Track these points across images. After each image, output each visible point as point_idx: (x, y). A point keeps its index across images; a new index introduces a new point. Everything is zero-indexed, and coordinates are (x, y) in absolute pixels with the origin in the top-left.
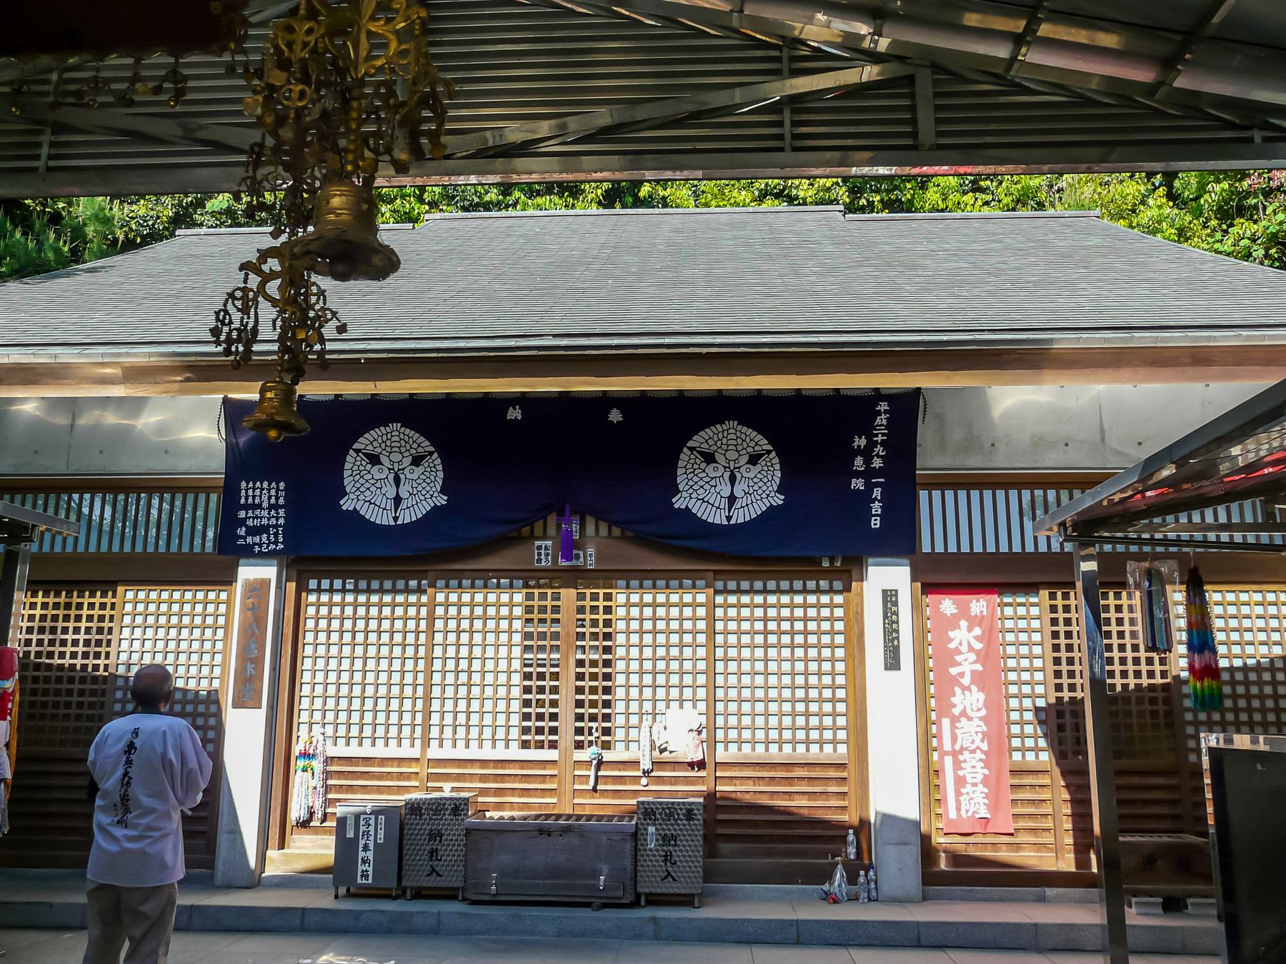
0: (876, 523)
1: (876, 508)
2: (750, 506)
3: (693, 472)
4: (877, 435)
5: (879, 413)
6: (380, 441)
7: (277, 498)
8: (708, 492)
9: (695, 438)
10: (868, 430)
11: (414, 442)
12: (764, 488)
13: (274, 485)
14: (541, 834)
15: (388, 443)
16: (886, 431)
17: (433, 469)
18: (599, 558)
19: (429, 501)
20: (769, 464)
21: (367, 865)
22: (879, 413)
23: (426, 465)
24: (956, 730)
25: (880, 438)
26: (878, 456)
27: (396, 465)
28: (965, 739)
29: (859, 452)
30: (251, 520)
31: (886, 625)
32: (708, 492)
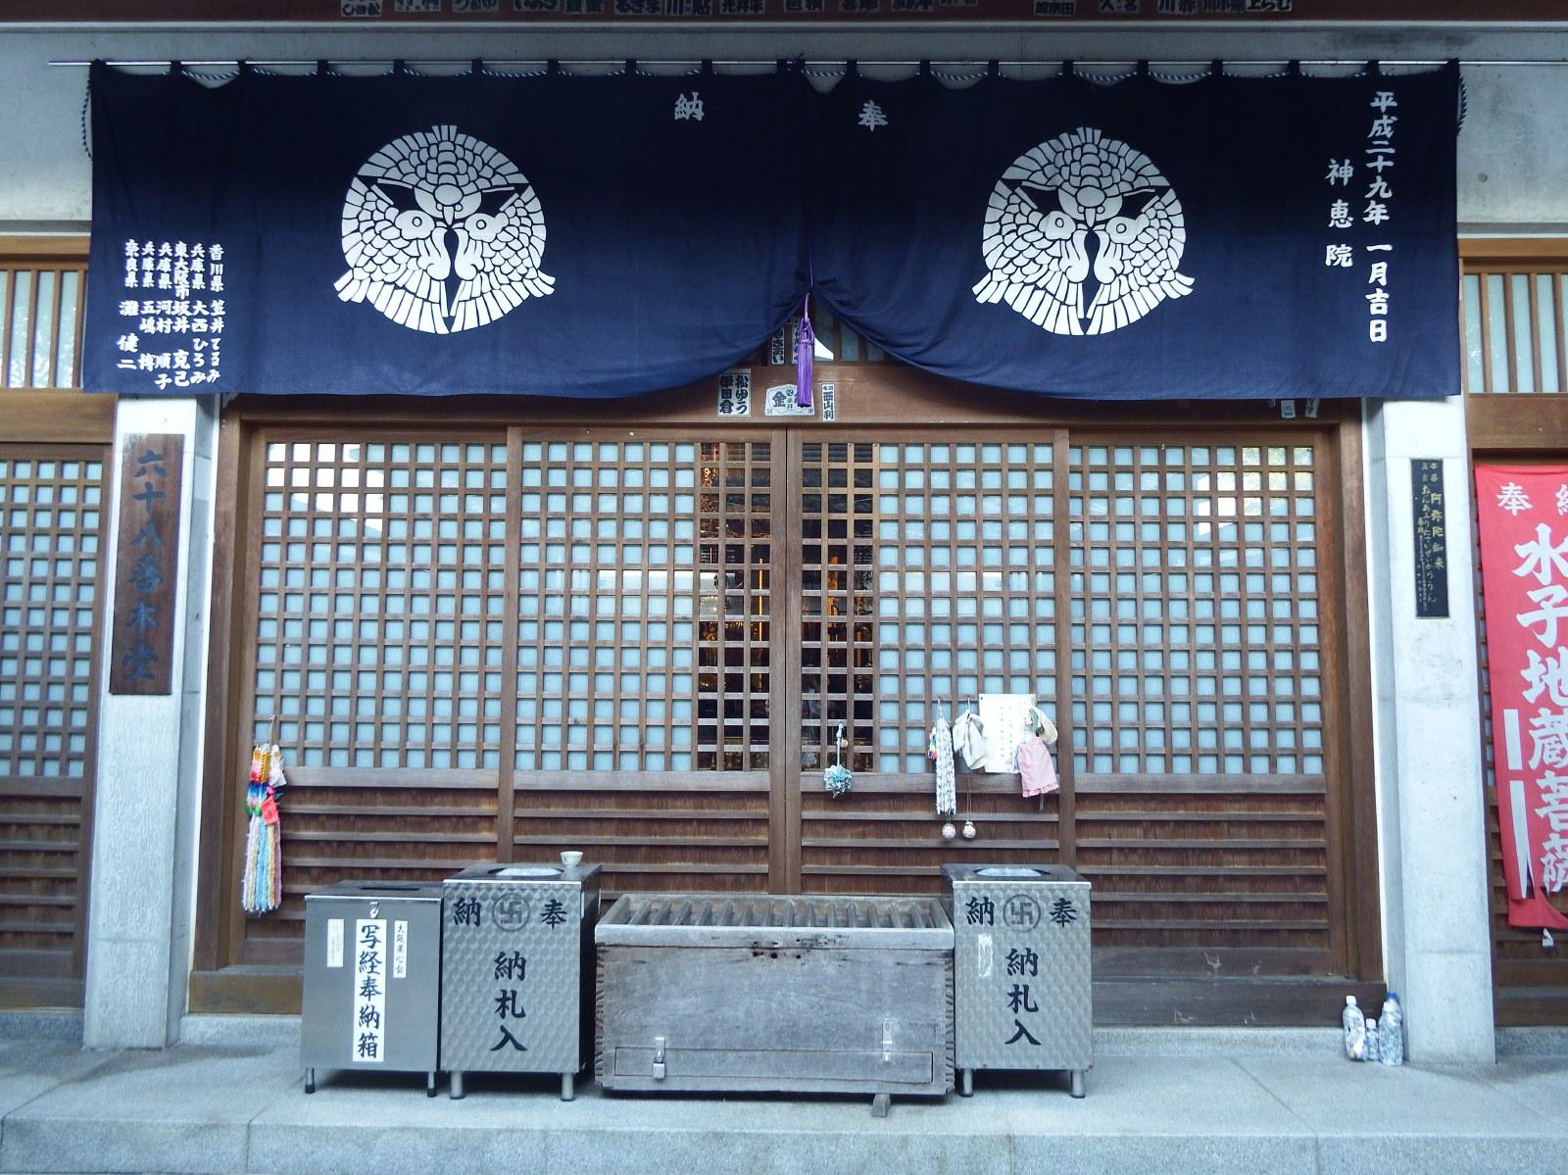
0: (1378, 332)
1: (1378, 302)
2: (1127, 299)
3: (1016, 231)
4: (1374, 158)
5: (1377, 113)
6: (414, 160)
7: (207, 278)
8: (403, 267)
9: (1021, 161)
10: (1357, 149)
11: (484, 164)
12: (515, 261)
13: (198, 249)
14: (755, 954)
15: (432, 165)
16: (1391, 151)
17: (1165, 223)
18: (844, 402)
19: (518, 286)
20: (1162, 214)
21: (373, 1023)
22: (1377, 113)
23: (511, 211)
24: (1531, 732)
25: (1380, 164)
26: (1378, 199)
27: (1090, 214)
28: (1547, 747)
29: (1339, 191)
30: (151, 319)
31: (1420, 530)
32: (403, 267)
